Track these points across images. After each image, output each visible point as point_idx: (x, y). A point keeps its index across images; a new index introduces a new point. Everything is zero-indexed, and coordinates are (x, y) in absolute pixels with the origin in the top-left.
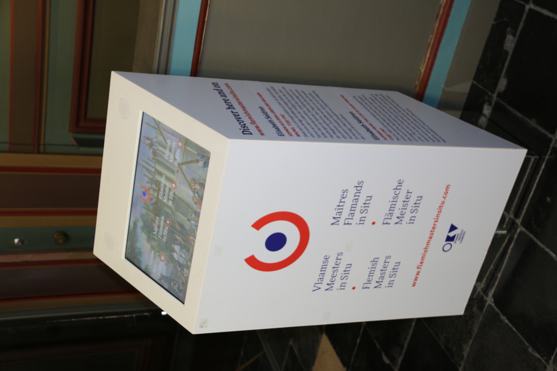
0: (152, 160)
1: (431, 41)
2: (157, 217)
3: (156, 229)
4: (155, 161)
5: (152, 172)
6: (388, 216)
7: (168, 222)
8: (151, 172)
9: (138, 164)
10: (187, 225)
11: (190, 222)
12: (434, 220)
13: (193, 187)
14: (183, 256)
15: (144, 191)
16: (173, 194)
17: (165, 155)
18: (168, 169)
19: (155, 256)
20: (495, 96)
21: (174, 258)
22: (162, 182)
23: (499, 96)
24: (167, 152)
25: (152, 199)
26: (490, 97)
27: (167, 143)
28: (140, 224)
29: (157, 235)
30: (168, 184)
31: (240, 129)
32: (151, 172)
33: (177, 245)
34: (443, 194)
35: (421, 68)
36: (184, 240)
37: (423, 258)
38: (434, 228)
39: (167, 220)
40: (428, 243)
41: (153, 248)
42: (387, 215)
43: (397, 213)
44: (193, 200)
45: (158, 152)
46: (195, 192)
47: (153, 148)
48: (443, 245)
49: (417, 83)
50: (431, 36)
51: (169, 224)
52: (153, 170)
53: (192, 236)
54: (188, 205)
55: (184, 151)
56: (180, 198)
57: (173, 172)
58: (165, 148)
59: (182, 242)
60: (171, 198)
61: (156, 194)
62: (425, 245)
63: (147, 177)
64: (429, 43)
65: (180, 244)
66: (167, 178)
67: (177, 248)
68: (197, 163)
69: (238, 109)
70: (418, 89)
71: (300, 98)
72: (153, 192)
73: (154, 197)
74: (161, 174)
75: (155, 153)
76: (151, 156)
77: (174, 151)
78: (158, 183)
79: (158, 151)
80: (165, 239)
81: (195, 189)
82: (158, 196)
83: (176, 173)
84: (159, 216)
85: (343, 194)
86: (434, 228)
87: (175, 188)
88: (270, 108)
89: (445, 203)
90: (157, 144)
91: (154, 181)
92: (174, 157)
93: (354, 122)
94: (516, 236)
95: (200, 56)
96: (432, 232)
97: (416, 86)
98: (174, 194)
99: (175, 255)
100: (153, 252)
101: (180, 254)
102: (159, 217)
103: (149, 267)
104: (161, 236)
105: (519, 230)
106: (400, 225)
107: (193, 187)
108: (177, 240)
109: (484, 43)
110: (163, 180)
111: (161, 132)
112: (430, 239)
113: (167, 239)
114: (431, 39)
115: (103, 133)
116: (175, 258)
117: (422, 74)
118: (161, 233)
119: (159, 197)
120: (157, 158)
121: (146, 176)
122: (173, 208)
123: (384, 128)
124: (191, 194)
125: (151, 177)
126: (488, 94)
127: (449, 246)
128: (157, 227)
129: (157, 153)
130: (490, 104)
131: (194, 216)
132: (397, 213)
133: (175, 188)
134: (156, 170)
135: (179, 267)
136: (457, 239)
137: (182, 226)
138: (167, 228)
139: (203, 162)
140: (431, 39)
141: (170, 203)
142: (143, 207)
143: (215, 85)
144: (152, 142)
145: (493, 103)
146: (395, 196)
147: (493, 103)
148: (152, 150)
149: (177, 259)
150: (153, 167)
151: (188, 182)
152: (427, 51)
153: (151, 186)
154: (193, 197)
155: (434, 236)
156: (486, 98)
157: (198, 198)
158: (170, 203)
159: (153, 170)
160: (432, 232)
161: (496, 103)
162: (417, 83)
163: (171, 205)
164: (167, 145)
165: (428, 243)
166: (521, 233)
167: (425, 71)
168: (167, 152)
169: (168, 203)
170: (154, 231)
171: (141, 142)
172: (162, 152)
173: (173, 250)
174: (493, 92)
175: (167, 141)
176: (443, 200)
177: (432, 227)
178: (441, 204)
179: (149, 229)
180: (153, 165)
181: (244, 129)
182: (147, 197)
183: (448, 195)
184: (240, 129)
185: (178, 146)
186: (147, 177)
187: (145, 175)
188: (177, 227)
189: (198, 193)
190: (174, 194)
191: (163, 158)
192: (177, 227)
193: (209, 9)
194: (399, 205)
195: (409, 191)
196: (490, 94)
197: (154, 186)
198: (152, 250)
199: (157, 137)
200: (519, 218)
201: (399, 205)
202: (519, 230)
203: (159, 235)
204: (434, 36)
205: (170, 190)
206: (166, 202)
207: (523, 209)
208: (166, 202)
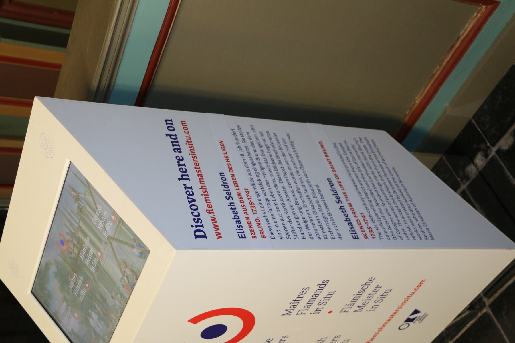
0: (76, 215)
1: (436, 73)
2: (75, 273)
3: (72, 284)
4: (79, 218)
5: (75, 227)
6: (348, 306)
7: (87, 285)
8: (73, 226)
9: (58, 209)
10: (110, 302)
11: (114, 300)
12: (397, 307)
13: (123, 270)
14: (101, 327)
15: (62, 239)
16: (97, 262)
17: (93, 218)
18: (95, 235)
19: (67, 309)
20: (494, 149)
21: (89, 323)
22: (86, 242)
23: (499, 152)
24: (96, 218)
25: (71, 253)
26: (488, 148)
27: (97, 208)
28: (53, 269)
29: (73, 291)
30: (92, 249)
31: (192, 226)
32: (73, 226)
33: (95, 313)
34: (415, 287)
35: (417, 98)
36: (104, 313)
37: (375, 336)
38: (395, 313)
39: (87, 283)
40: (385, 325)
41: (65, 299)
42: (347, 305)
43: (359, 303)
44: (121, 282)
45: (84, 210)
46: (124, 275)
47: (79, 203)
48: (401, 325)
49: (407, 113)
50: (438, 67)
51: (88, 288)
52: (76, 225)
53: (114, 314)
54: (114, 283)
55: (116, 230)
56: (104, 270)
57: (101, 241)
58: (95, 212)
59: (101, 313)
60: (94, 265)
61: (76, 251)
62: (381, 326)
63: (69, 229)
64: (434, 75)
65: (98, 314)
66: (91, 242)
67: (94, 315)
68: (132, 248)
69: (194, 182)
70: (407, 119)
71: (271, 149)
72: (73, 247)
73: (74, 252)
74: (86, 235)
75: (80, 209)
76: (76, 210)
77: (104, 220)
78: (81, 243)
79: (84, 209)
80: (81, 299)
81: (125, 272)
82: (79, 252)
83: (103, 243)
84: (77, 273)
85: (303, 291)
86: (395, 313)
87: (100, 258)
88: (233, 176)
89: (415, 294)
90: (84, 202)
91: (76, 236)
92: (104, 226)
93: (330, 199)
94: (479, 315)
95: (155, 71)
96: (392, 316)
97: (405, 116)
98: (99, 262)
99: (91, 321)
100: (65, 304)
101: (97, 323)
102: (77, 275)
103: (58, 315)
104: (76, 293)
105: (484, 310)
106: (360, 312)
107: (123, 270)
108: (96, 309)
109: (496, 81)
110: (87, 241)
111: (91, 191)
112: (388, 321)
113: (83, 299)
114: (437, 70)
115: (22, 138)
116: (91, 324)
117: (415, 106)
118: (78, 292)
119: (80, 256)
120: (82, 215)
121: (66, 225)
122: (96, 276)
123: (366, 214)
124: (120, 275)
125: (73, 231)
126: (486, 144)
127: (407, 325)
128: (74, 283)
129: (82, 210)
130: (486, 156)
131: (119, 297)
132: (359, 303)
133: (100, 258)
134: (80, 227)
135: (94, 334)
136: (417, 320)
137: (104, 300)
138: (86, 290)
139: (140, 251)
140: (438, 71)
141: (93, 269)
142: (59, 255)
143: (169, 123)
144: (78, 196)
145: (490, 156)
146: (362, 290)
147: (490, 156)
148: (77, 204)
149: (93, 326)
150: (77, 223)
151: (117, 260)
152: (429, 82)
153: (71, 239)
154: (122, 279)
155: (393, 320)
156: (483, 146)
157: (127, 282)
158: (93, 269)
159: (76, 225)
160: (392, 316)
161: (493, 158)
162: (407, 113)
163: (93, 271)
164: (97, 210)
165: (385, 325)
166: (485, 314)
167: (420, 103)
168: (96, 218)
169: (90, 268)
170: (70, 285)
171: (64, 188)
172: (91, 215)
173: (90, 316)
174: (493, 145)
175: (97, 206)
176: (414, 291)
177: (394, 311)
178: (410, 295)
179: (64, 279)
180: (78, 221)
181: (197, 226)
182: (64, 247)
183: (420, 288)
184: (192, 226)
185: (111, 218)
186: (69, 229)
187: (65, 224)
188: (98, 296)
189: (127, 277)
190: (99, 262)
191: (91, 220)
192: (98, 296)
193: (175, 20)
194: (365, 296)
195: (378, 286)
196: (488, 144)
197: (75, 242)
198: (64, 302)
199: (85, 194)
200: (489, 298)
201: (365, 296)
202: (484, 310)
203: (75, 292)
204: (442, 68)
205: (94, 256)
206: (88, 265)
207: (496, 292)
208: (88, 265)
